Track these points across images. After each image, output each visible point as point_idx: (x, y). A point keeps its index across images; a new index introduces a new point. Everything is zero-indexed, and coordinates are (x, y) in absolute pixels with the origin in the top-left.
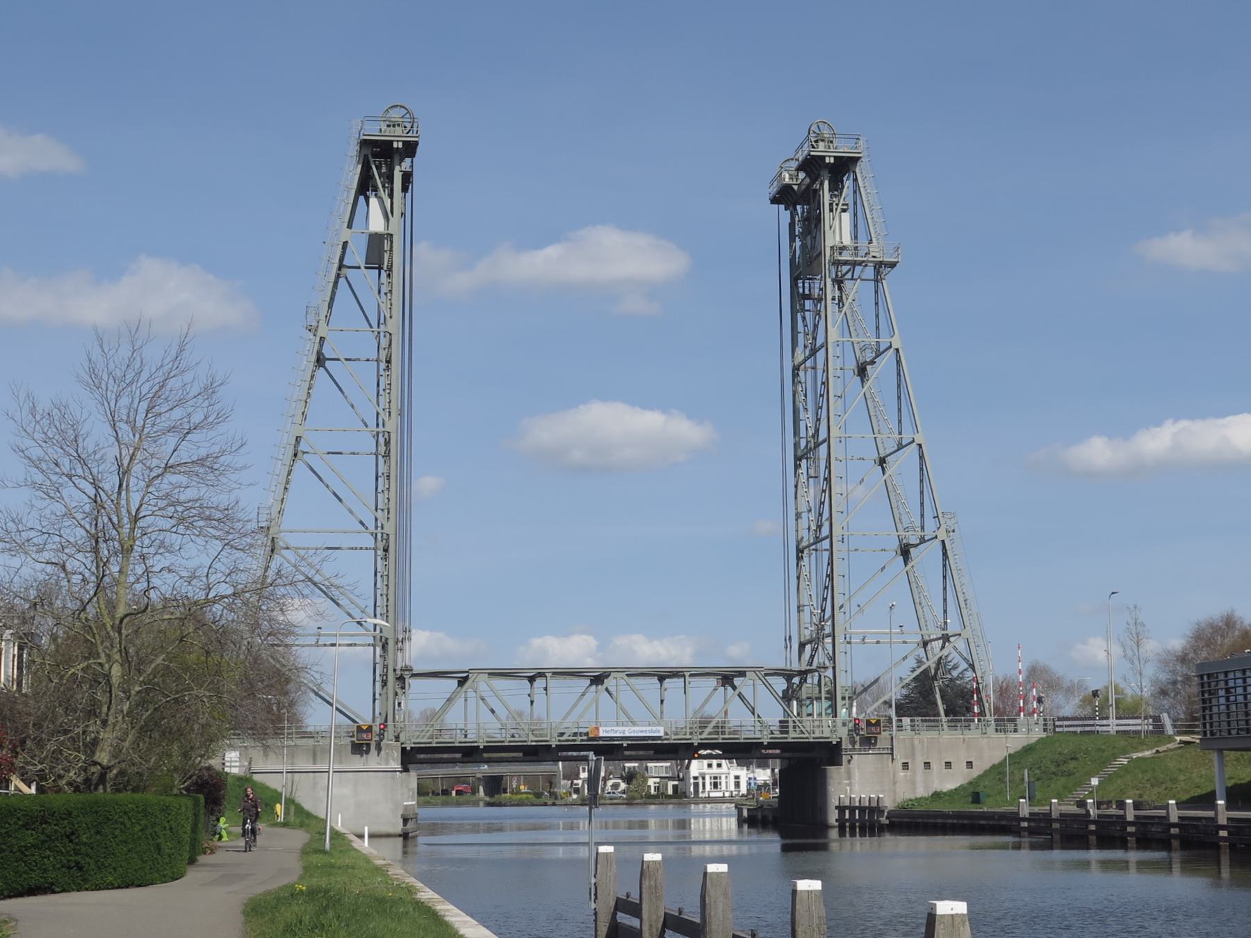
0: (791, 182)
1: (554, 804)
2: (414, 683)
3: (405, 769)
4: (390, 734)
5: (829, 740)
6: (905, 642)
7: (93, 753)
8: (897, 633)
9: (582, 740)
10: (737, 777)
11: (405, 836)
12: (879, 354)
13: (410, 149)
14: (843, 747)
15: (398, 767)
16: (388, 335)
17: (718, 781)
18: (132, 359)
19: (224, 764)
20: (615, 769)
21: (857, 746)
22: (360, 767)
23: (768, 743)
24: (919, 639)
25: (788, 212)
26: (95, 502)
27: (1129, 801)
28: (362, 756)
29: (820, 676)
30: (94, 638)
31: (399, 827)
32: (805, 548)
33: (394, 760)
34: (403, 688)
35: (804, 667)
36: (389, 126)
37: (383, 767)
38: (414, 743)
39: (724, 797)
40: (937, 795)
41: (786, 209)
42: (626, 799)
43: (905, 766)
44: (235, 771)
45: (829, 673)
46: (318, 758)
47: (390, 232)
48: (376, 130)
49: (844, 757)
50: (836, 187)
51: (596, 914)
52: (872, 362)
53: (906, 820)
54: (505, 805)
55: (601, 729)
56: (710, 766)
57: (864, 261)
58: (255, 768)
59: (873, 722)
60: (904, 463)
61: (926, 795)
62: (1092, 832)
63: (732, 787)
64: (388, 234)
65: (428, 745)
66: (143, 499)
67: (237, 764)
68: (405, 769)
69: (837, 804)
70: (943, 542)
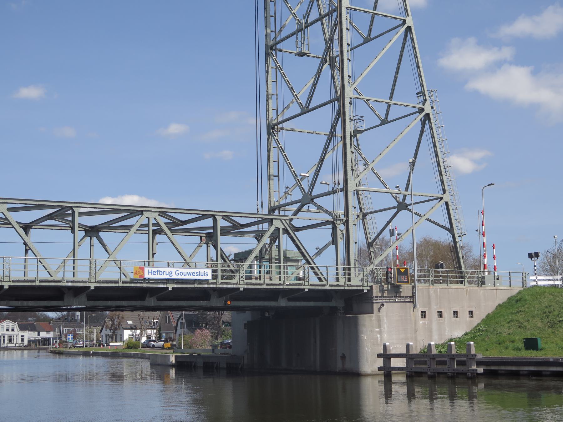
5: (361, 288)
10: (22, 336)
14: (374, 295)
17: (12, 338)
21: (386, 295)
23: (96, 287)
39: (15, 346)
43: (424, 314)
49: (375, 305)
55: (147, 269)
63: (19, 341)
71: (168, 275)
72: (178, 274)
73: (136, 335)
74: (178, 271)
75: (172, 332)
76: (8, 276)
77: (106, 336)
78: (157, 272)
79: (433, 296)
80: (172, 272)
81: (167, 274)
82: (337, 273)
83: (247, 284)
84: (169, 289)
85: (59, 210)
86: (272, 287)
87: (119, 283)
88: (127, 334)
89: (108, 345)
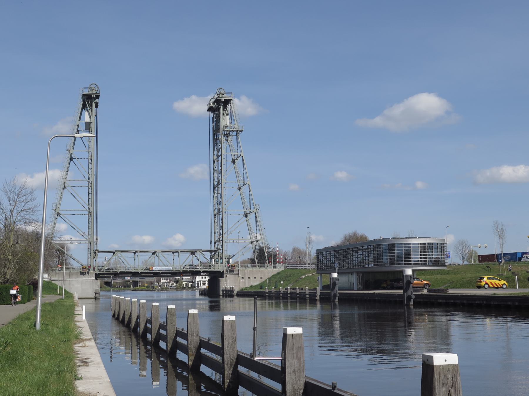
0: (213, 105)
1: (153, 290)
2: (98, 254)
3: (96, 279)
4: (92, 269)
6: (245, 242)
7: (6, 276)
8: (241, 240)
9: (148, 271)
11: (95, 298)
12: (238, 157)
13: (98, 97)
15: (94, 278)
16: (91, 152)
17: (205, 283)
18: (13, 186)
20: (172, 279)
21: (228, 272)
22: (83, 279)
24: (250, 241)
25: (212, 114)
26: (5, 218)
27: (297, 288)
28: (83, 275)
29: (218, 252)
30: (5, 249)
31: (93, 296)
32: (216, 214)
33: (93, 277)
34: (96, 256)
35: (215, 250)
36: (91, 90)
37: (90, 279)
40: (251, 287)
41: (212, 113)
42: (176, 288)
44: (46, 280)
45: (221, 251)
47: (91, 122)
48: (87, 92)
49: (225, 276)
50: (225, 107)
51: (112, 309)
52: (237, 159)
53: (242, 294)
54: (137, 290)
55: (153, 268)
56: (202, 278)
57: (233, 130)
60: (245, 189)
61: (248, 287)
62: (281, 296)
64: (91, 122)
66: (16, 218)
68: (96, 279)
69: (222, 289)
70: (255, 213)
79: (246, 273)
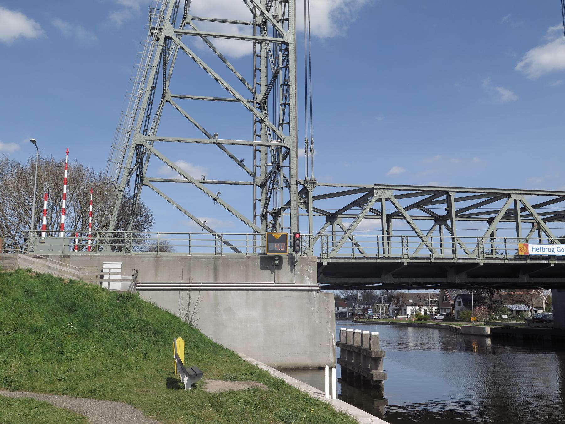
19: (102, 277)
28: (272, 272)
33: (310, 278)
38: (331, 258)
44: (115, 286)
46: (221, 273)
55: (530, 246)
58: (144, 281)
59: (277, 237)
65: (346, 261)
67: (119, 277)
71: (550, 251)
72: (560, 250)
73: (416, 310)
74: (559, 247)
75: (449, 308)
76: (327, 253)
77: (393, 311)
78: (540, 248)
80: (554, 249)
81: (549, 250)
82: (254, 241)
83: (487, 259)
84: (552, 265)
85: (431, 196)
86: (366, 261)
87: (505, 260)
88: (409, 309)
89: (396, 318)
